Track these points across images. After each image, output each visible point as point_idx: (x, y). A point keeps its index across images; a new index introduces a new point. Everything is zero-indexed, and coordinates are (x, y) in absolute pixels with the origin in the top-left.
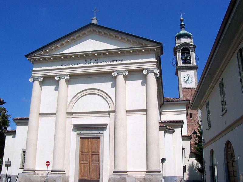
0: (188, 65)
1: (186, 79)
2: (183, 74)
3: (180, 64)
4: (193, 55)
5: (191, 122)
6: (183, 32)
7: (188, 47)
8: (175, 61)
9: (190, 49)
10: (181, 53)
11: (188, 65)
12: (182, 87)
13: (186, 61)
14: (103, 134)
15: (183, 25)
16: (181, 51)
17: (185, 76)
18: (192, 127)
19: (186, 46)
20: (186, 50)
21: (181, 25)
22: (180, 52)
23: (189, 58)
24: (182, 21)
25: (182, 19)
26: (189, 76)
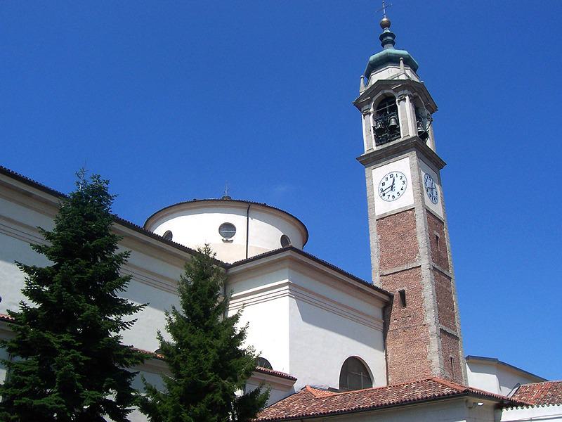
0: (397, 141)
2: (377, 175)
3: (370, 144)
4: (405, 110)
5: (404, 322)
6: (390, 50)
7: (391, 92)
8: (437, 221)
9: (396, 96)
10: (372, 115)
11: (397, 141)
12: (377, 214)
13: (387, 131)
15: (387, 34)
16: (372, 110)
18: (407, 339)
19: (386, 91)
20: (386, 106)
22: (370, 114)
23: (393, 123)
24: (384, 26)
25: (385, 20)
26: (395, 175)
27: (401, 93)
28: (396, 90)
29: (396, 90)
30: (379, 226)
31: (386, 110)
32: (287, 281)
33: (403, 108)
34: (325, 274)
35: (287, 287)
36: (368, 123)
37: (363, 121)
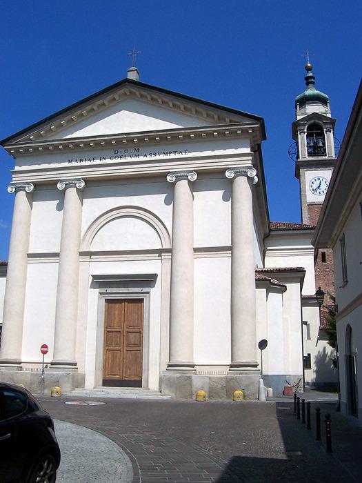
0: (320, 158)
1: (315, 186)
2: (309, 176)
3: (304, 155)
5: (324, 271)
9: (324, 126)
11: (320, 158)
13: (316, 149)
14: (107, 383)
16: (306, 130)
17: (314, 181)
19: (317, 121)
21: (307, 78)
22: (304, 133)
23: (321, 145)
24: (308, 69)
25: (309, 65)
26: (321, 179)
27: (329, 126)
28: (325, 123)
29: (325, 123)
30: (309, 209)
31: (313, 133)
32: (248, 150)
33: (328, 137)
34: (284, 235)
35: (251, 158)
36: (303, 139)
37: (299, 136)
